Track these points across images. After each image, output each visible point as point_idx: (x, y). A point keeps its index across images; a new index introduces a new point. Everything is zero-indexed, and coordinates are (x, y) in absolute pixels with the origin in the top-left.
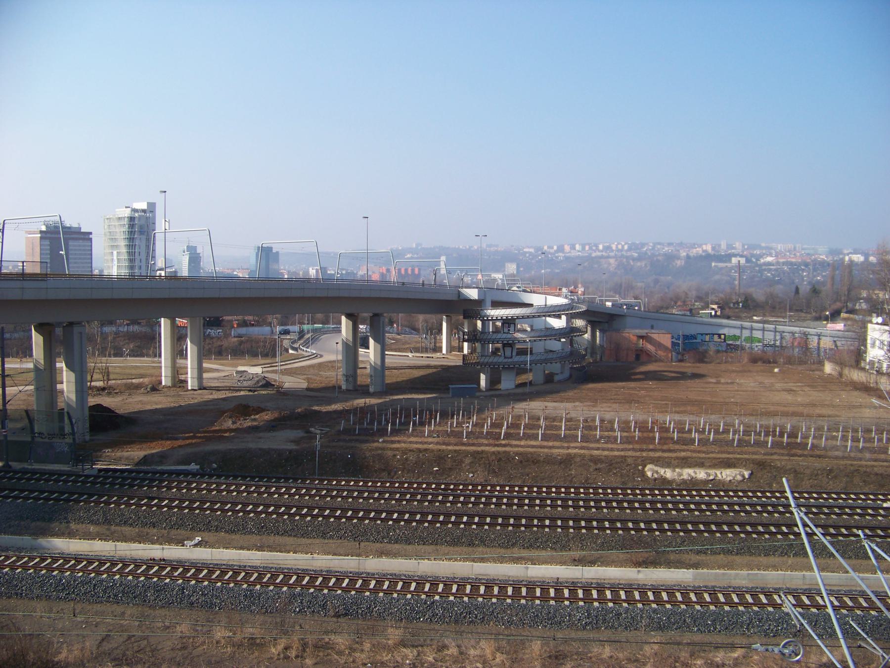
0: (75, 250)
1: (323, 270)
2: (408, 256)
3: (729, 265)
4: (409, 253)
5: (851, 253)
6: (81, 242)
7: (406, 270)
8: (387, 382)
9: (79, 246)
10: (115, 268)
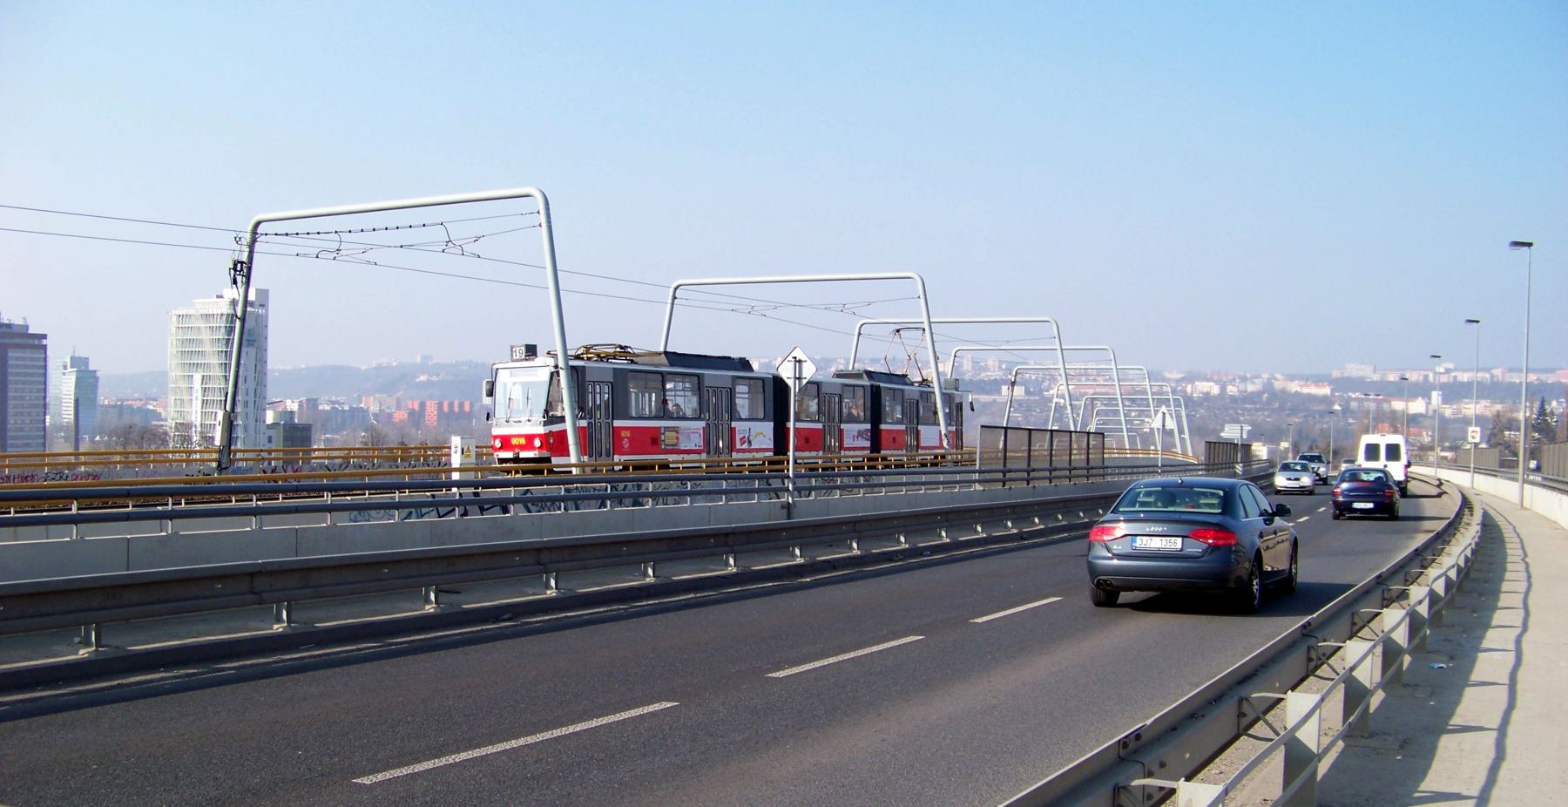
0: (18, 366)
1: (313, 403)
2: (423, 378)
3: (997, 397)
4: (423, 373)
5: (1455, 370)
6: (28, 354)
7: (451, 405)
8: (1297, 734)
9: (24, 359)
10: (197, 405)
